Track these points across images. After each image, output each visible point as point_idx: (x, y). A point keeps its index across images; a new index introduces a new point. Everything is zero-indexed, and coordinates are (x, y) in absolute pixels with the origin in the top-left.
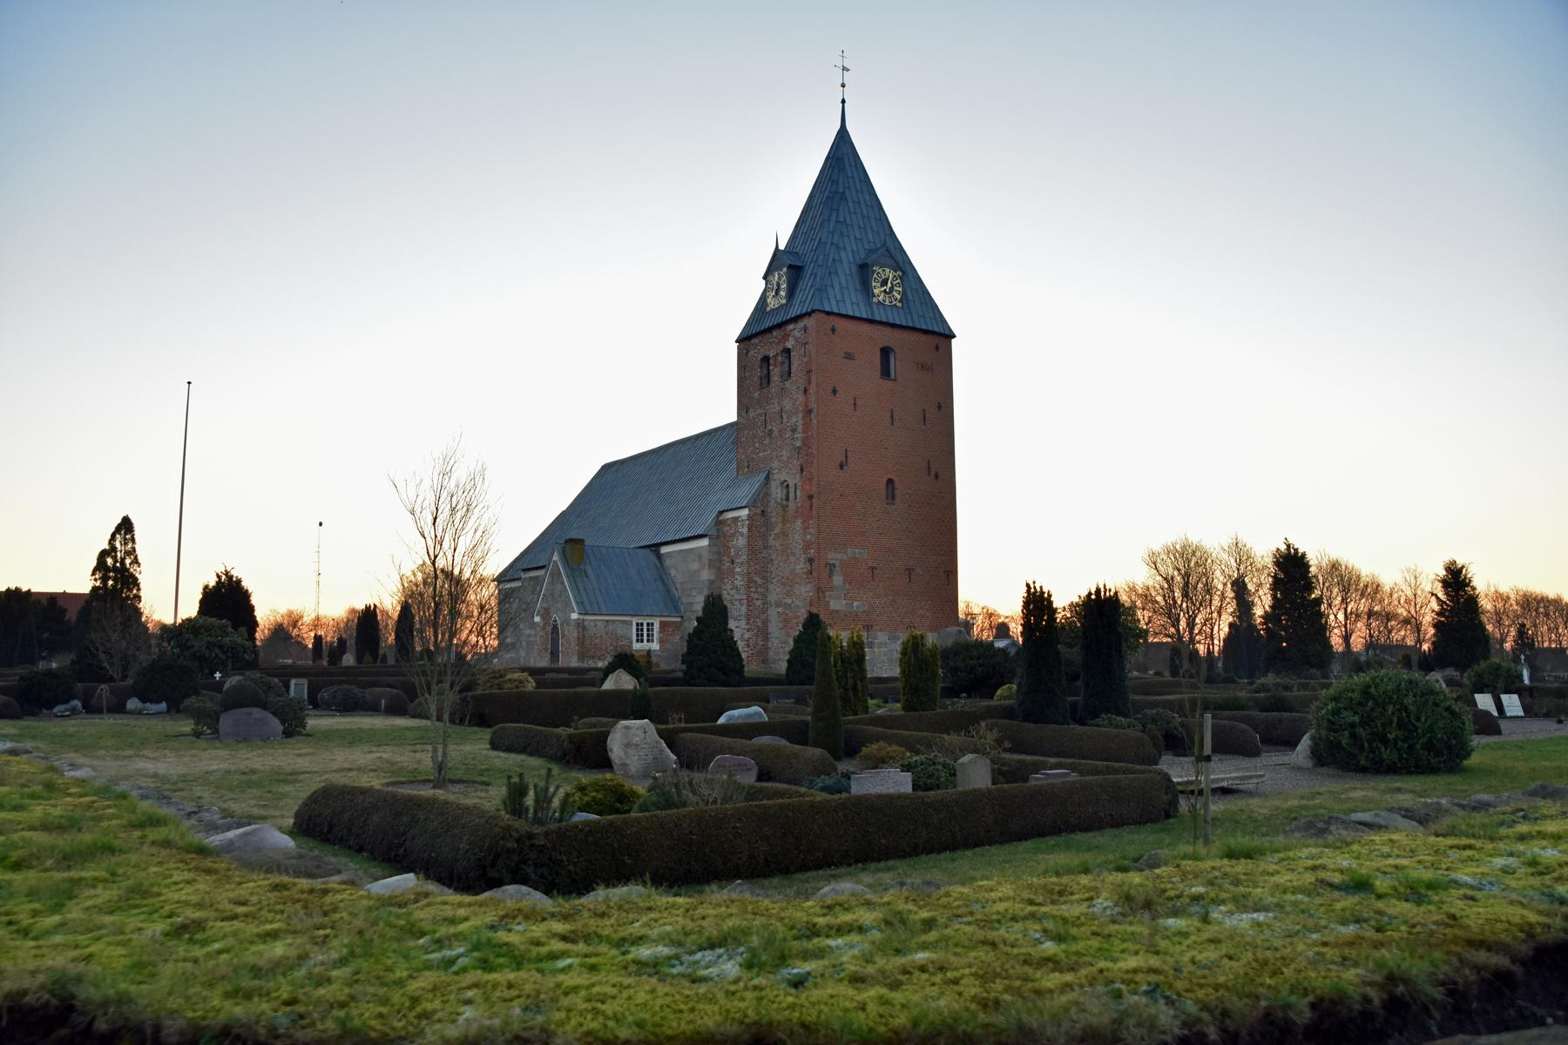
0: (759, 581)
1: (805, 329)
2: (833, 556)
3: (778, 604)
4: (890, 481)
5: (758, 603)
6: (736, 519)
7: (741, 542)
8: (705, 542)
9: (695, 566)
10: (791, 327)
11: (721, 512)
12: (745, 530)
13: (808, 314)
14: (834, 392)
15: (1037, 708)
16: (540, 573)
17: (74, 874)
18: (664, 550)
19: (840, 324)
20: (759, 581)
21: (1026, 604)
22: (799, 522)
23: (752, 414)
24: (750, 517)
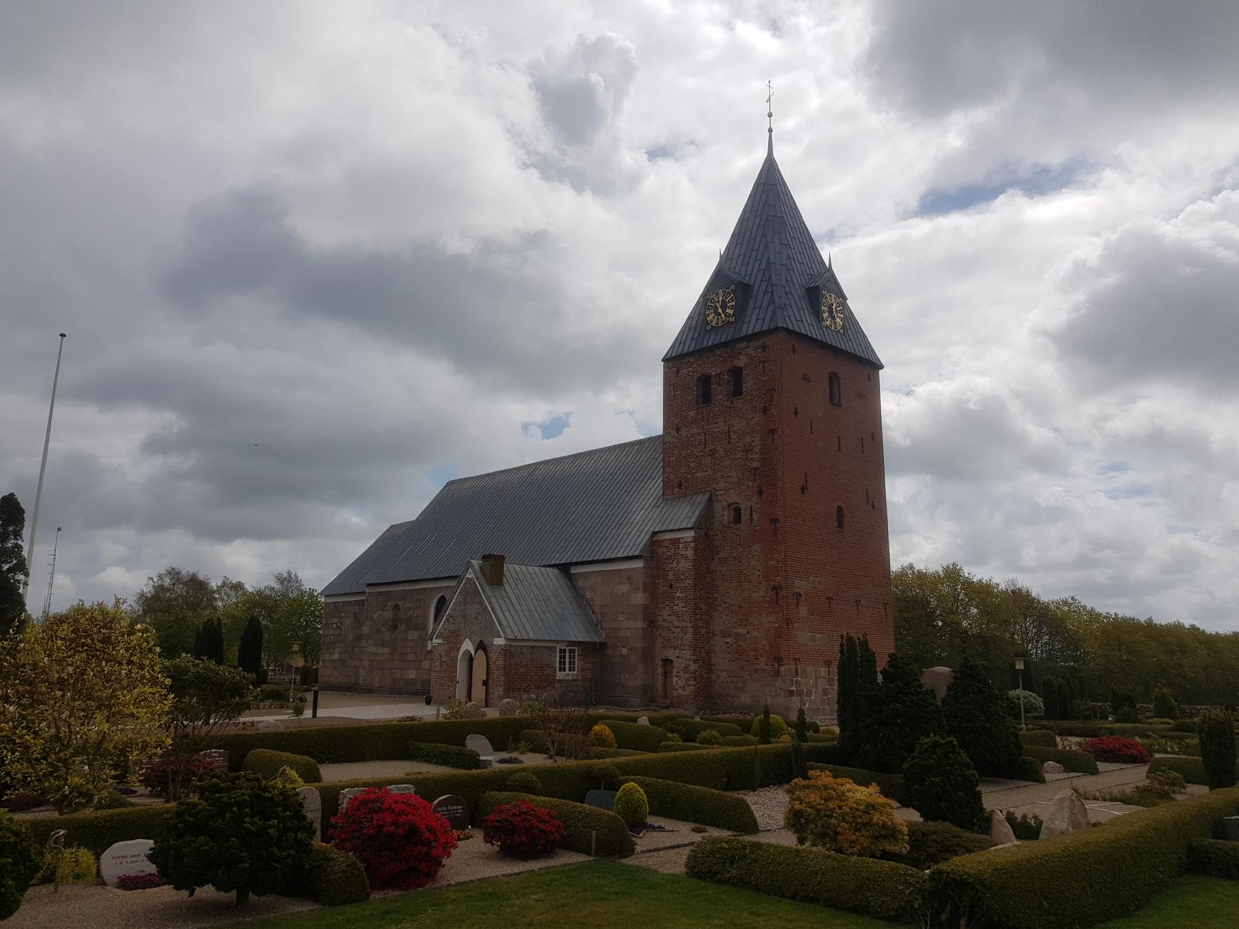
0: (704, 608)
1: (764, 347)
2: (800, 585)
3: (725, 634)
4: (840, 509)
5: (703, 631)
6: (676, 542)
7: (685, 566)
8: (639, 564)
9: (624, 588)
10: (743, 345)
11: (655, 533)
12: (690, 553)
13: (770, 332)
14: (796, 413)
15: (733, 856)
16: (453, 583)
17: (592, 712)
18: (574, 570)
19: (765, 340)
20: (704, 608)
21: (319, 774)
22: (756, 548)
23: (684, 433)
24: (696, 539)
